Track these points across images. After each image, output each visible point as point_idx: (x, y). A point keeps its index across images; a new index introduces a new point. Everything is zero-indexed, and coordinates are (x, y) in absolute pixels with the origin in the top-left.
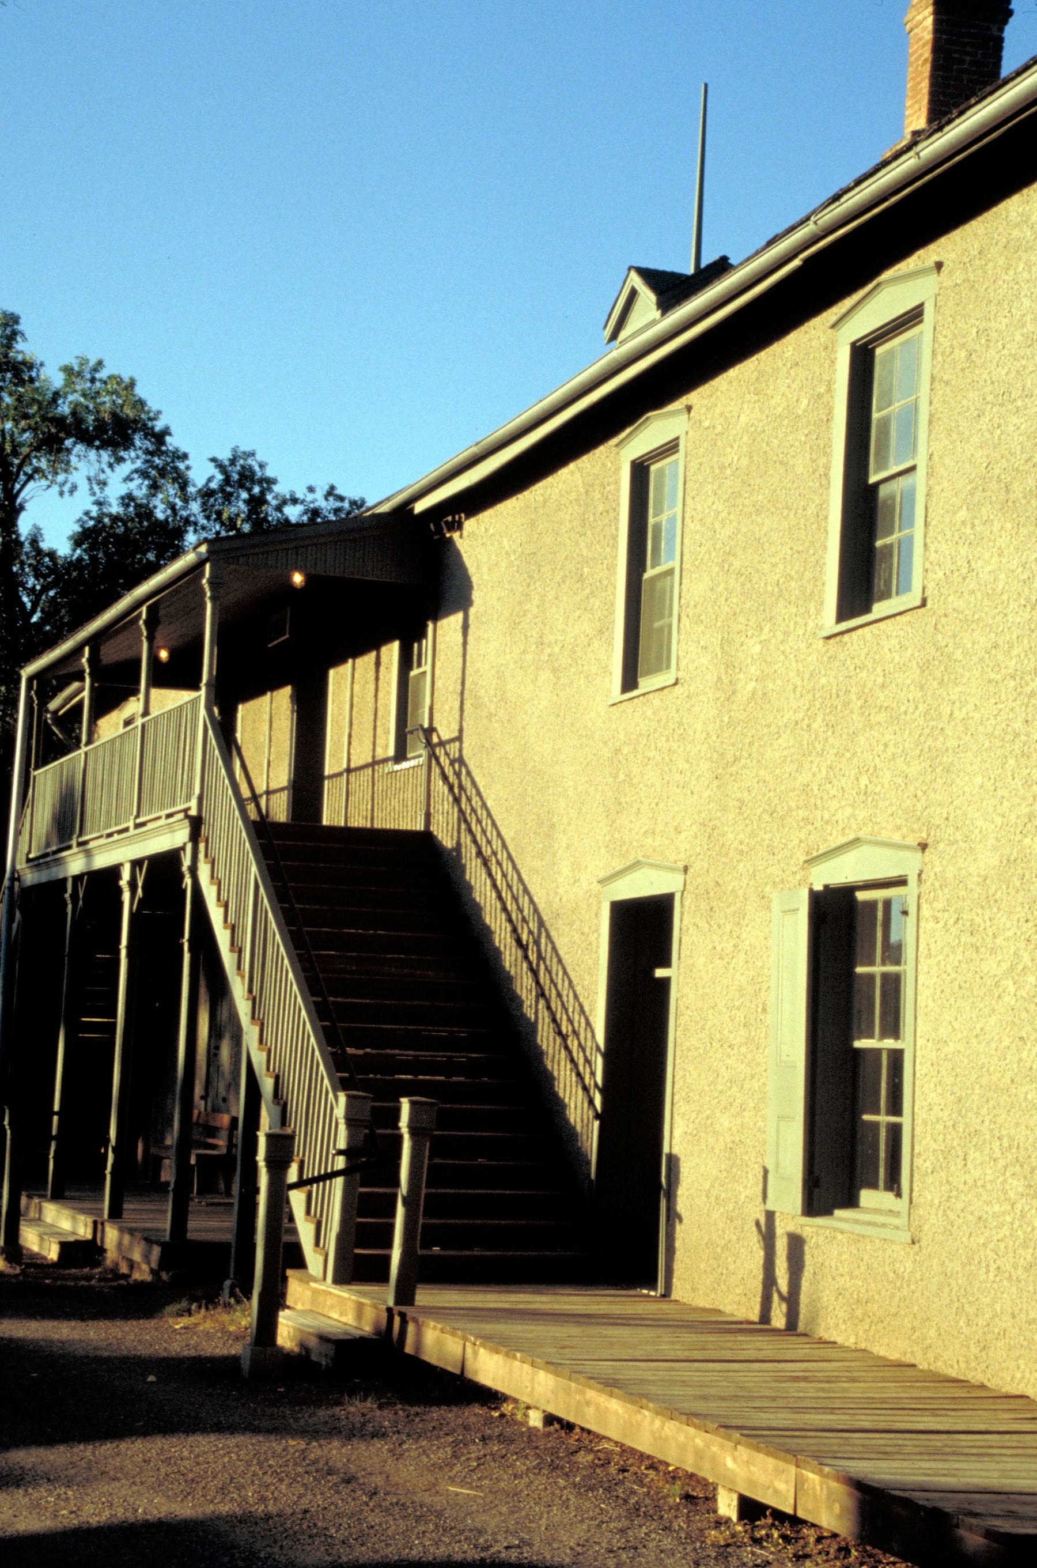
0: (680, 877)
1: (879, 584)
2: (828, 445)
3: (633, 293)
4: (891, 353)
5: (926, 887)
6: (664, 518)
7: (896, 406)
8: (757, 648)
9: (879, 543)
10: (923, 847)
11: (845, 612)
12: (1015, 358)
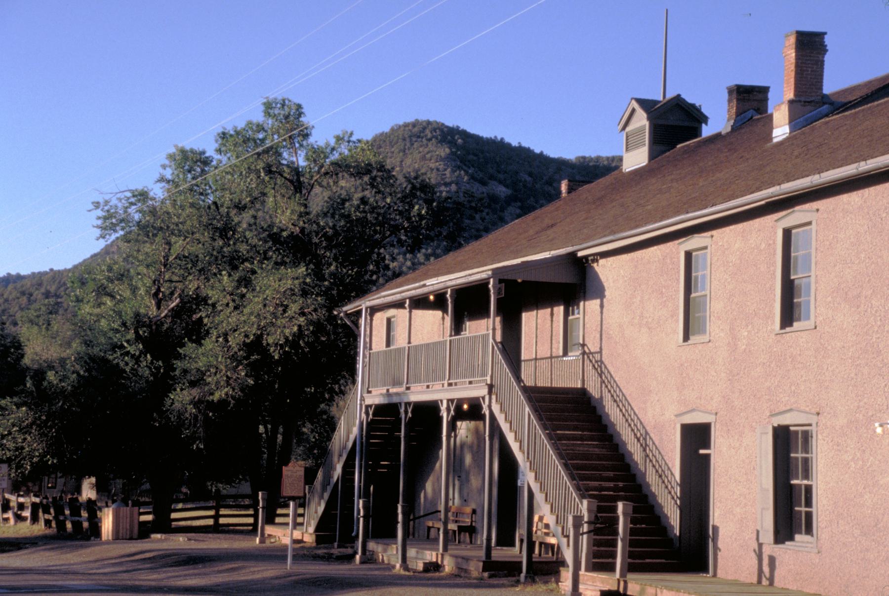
0: (714, 417)
1: (796, 315)
2: (775, 262)
3: (633, 111)
4: (798, 233)
5: (819, 428)
6: (700, 274)
7: (801, 253)
8: (746, 333)
9: (795, 300)
10: (818, 414)
11: (783, 327)
12: (848, 249)
